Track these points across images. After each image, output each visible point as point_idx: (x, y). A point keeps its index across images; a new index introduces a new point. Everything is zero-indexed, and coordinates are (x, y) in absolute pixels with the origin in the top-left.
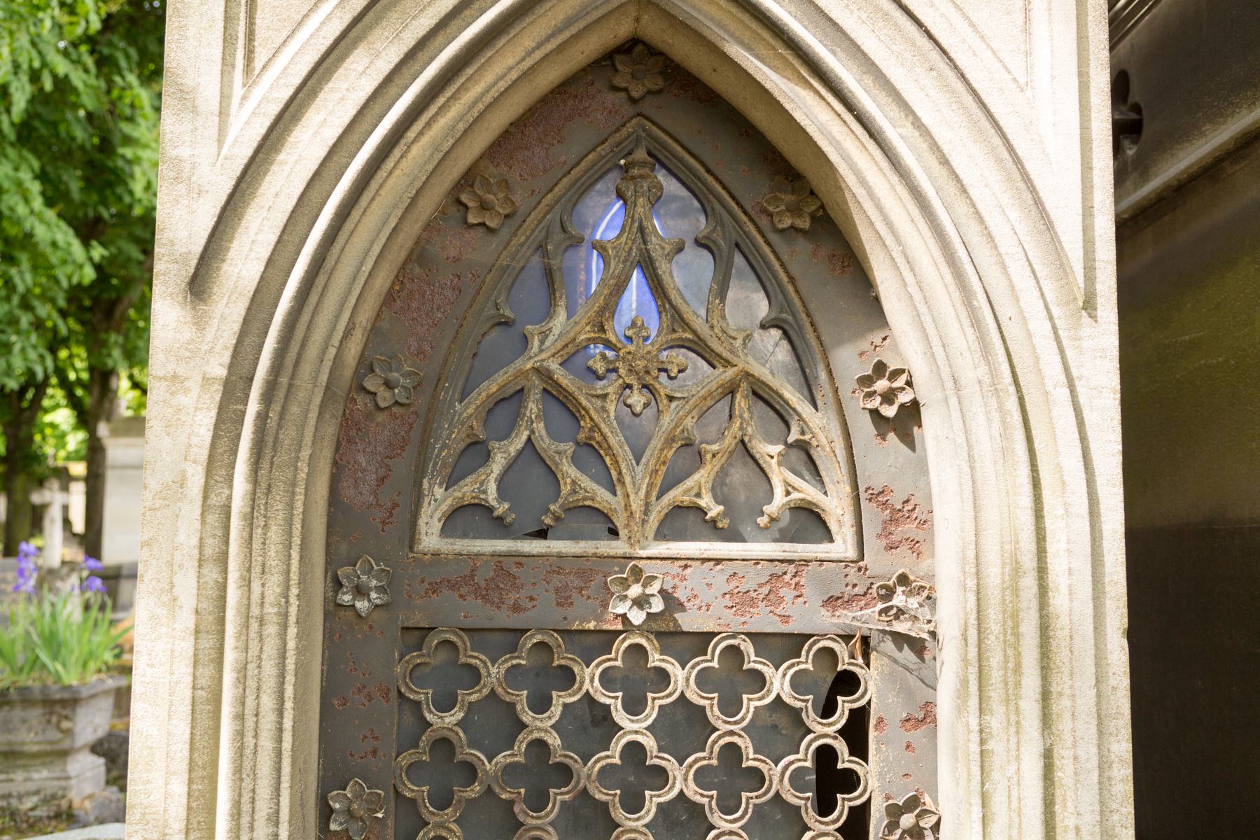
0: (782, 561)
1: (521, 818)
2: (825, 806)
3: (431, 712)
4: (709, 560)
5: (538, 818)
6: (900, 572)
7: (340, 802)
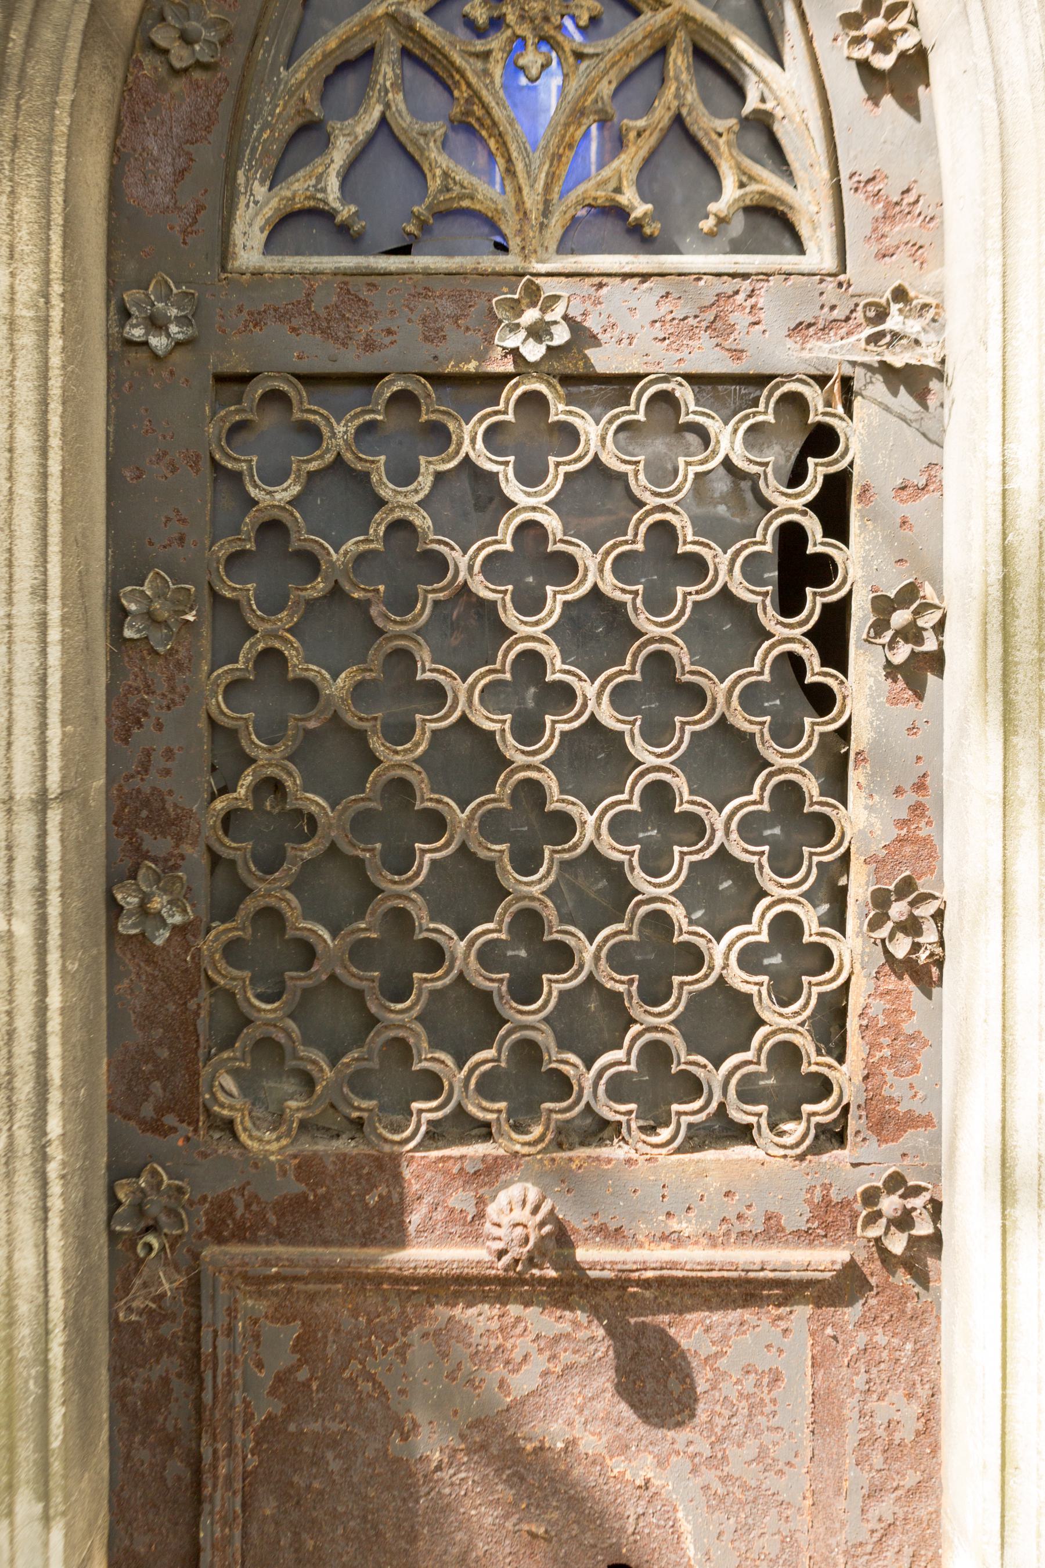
0: (733, 276)
1: (380, 623)
2: (789, 603)
3: (256, 486)
4: (632, 275)
5: (403, 623)
6: (896, 284)
7: (136, 602)
